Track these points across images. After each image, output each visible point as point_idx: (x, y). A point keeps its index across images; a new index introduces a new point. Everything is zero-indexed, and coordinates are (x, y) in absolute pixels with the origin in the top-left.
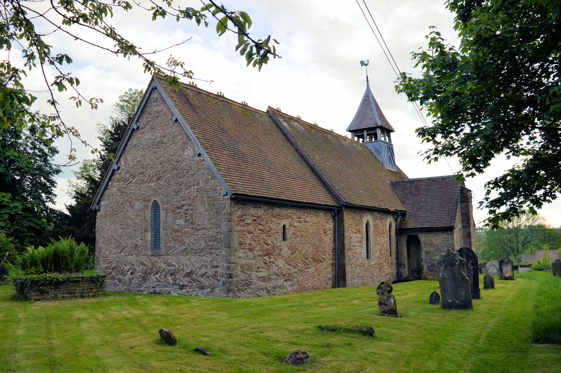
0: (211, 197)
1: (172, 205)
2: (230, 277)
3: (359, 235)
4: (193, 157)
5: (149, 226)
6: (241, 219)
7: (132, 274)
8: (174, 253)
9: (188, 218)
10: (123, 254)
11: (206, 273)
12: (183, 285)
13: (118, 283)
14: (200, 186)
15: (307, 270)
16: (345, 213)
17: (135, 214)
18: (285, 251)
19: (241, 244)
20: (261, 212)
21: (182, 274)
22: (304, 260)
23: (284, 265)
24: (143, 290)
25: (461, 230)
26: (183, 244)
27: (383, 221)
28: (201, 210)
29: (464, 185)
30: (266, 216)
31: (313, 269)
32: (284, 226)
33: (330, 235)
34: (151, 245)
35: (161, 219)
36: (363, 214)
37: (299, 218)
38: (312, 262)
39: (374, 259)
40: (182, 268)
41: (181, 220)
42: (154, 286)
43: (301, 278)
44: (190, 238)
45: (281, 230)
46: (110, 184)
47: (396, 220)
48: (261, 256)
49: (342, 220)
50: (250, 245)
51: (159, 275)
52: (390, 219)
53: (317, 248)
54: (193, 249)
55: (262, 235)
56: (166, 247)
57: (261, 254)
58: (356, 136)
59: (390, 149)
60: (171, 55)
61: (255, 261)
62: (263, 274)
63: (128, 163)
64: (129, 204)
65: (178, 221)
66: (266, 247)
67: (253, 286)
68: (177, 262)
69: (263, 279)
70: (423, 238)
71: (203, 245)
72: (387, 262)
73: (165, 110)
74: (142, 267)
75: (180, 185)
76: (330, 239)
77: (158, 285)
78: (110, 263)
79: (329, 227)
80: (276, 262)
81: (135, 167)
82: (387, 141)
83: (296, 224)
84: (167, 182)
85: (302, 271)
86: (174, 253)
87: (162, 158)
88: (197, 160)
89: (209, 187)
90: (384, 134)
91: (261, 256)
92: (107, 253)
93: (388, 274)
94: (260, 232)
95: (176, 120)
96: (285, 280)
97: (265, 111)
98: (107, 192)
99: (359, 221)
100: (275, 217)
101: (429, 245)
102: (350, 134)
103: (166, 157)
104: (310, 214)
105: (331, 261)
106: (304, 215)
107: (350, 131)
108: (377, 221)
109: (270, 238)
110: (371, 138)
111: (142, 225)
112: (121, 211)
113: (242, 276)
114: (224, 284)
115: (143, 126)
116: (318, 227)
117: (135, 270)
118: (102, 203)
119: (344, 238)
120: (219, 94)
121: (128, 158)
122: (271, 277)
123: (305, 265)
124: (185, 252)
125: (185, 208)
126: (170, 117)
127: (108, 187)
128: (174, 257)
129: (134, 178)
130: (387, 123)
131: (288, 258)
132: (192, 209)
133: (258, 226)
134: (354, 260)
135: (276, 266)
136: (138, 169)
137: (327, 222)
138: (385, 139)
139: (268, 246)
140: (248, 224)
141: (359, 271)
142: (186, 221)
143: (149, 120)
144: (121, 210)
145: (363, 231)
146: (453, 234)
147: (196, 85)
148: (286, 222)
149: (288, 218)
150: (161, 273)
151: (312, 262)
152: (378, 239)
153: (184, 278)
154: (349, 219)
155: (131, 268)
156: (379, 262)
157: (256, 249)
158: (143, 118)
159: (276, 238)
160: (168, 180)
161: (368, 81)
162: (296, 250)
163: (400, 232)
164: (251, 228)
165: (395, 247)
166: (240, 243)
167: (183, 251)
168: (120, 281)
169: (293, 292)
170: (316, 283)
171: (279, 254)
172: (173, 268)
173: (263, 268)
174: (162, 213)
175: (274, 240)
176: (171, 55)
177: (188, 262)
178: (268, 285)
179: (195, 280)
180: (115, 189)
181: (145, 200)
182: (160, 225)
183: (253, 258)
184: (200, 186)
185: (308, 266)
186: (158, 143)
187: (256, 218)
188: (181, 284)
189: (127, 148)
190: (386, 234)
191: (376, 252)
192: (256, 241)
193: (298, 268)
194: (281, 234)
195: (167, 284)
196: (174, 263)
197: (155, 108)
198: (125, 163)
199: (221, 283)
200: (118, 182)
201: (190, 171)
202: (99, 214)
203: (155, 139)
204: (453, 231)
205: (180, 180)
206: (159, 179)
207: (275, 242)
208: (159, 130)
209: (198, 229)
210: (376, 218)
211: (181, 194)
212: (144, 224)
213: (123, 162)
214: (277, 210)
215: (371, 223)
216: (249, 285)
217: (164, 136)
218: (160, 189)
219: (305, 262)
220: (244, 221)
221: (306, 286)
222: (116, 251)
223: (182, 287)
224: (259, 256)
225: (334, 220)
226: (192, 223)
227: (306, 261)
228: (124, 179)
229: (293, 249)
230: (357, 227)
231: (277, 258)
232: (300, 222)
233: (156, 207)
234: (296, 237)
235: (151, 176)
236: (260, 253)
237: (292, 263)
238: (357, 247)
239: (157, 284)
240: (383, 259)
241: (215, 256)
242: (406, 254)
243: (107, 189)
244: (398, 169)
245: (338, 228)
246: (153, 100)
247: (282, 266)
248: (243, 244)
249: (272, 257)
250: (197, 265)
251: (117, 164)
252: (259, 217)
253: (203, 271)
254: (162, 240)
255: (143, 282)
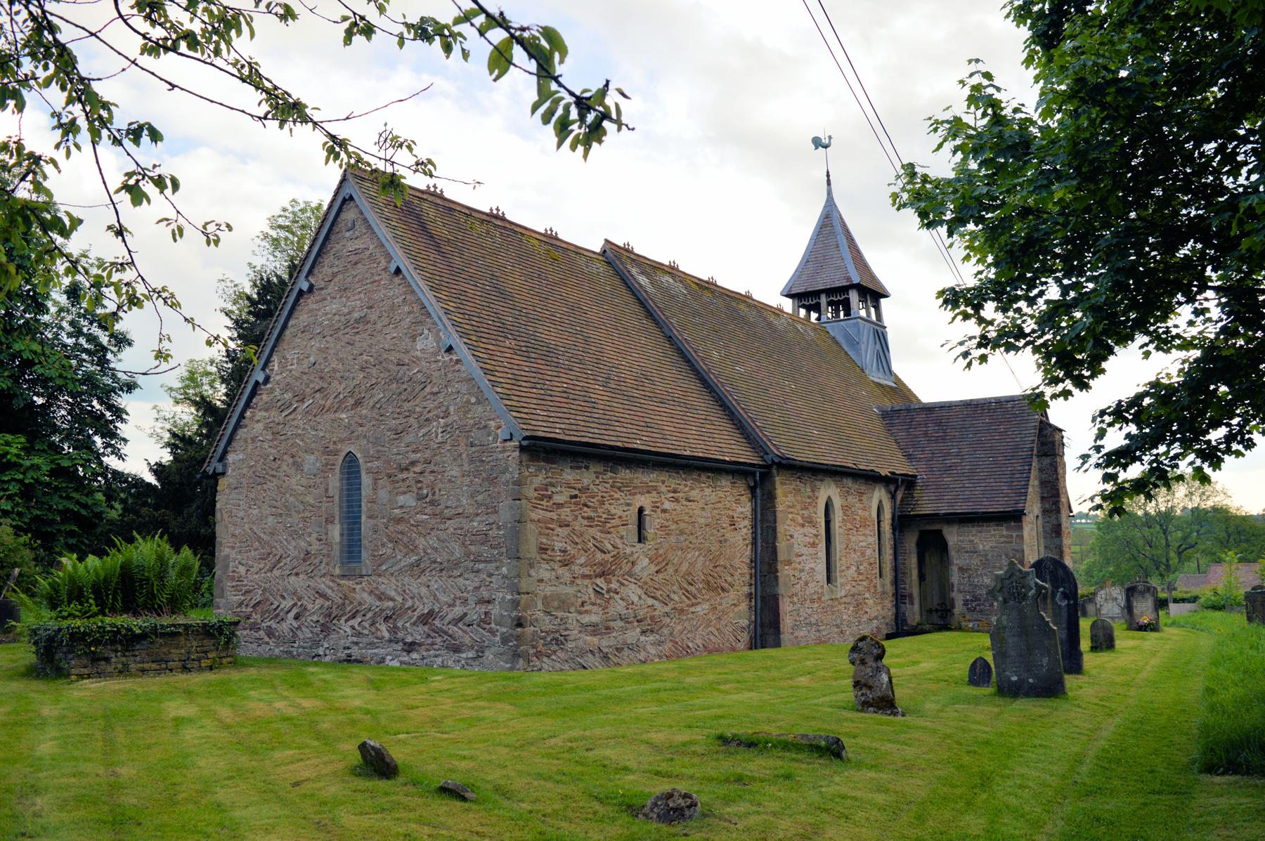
0: (476, 445)
1: (388, 462)
2: (520, 625)
3: (810, 530)
4: (435, 354)
5: (337, 509)
6: (544, 494)
7: (297, 617)
8: (391, 570)
9: (425, 492)
10: (276, 573)
11: (465, 615)
12: (413, 644)
13: (267, 639)
14: (450, 420)
15: (692, 609)
16: (778, 479)
17: (304, 482)
18: (644, 566)
19: (543, 550)
20: (589, 477)
21: (411, 618)
22: (686, 586)
23: (640, 598)
24: (321, 653)
25: (1040, 518)
26: (412, 551)
27: (864, 498)
28: (453, 473)
29: (1047, 418)
30: (599, 487)
31: (706, 606)
32: (641, 510)
33: (745, 531)
34: (341, 552)
35: (363, 493)
36: (818, 483)
37: (675, 491)
38: (704, 591)
39: (842, 585)
40: (409, 603)
41: (407, 496)
42: (347, 645)
43: (679, 627)
44: (428, 537)
45: (635, 518)
46: (248, 414)
47: (893, 497)
48: (589, 577)
49: (771, 497)
50: (564, 551)
51: (359, 620)
52: (879, 495)
53: (715, 559)
54: (435, 562)
55: (591, 530)
56: (375, 556)
57: (587, 573)
58: (804, 306)
59: (880, 336)
60: (386, 125)
61: (575, 588)
62: (594, 618)
63: (289, 367)
64: (291, 460)
65: (401, 499)
66: (599, 556)
67: (570, 645)
68: (399, 590)
69: (594, 629)
70: (953, 536)
71: (458, 552)
72: (872, 591)
73: (371, 247)
74: (320, 601)
75: (406, 417)
76: (745, 539)
77: (357, 643)
78: (247, 592)
79: (742, 513)
80: (622, 590)
81: (305, 377)
82: (874, 317)
83: (667, 505)
84: (376, 411)
85: (682, 611)
86: (391, 570)
87: (365, 357)
88: (444, 362)
89: (472, 421)
90: (866, 302)
91: (589, 577)
92: (242, 570)
93: (876, 618)
94: (586, 522)
95: (398, 271)
96: (643, 632)
97: (598, 250)
98: (241, 433)
99: (809, 497)
100: (619, 488)
101: (967, 552)
102: (789, 301)
103: (375, 355)
104: (699, 482)
105: (746, 589)
106: (686, 486)
107: (789, 296)
108: (850, 498)
109: (609, 536)
110: (837, 312)
111: (320, 507)
112: (273, 476)
113: (547, 623)
114: (505, 640)
115: (323, 284)
116: (716, 511)
117: (306, 609)
118: (231, 458)
119: (775, 538)
120: (495, 212)
121: (288, 356)
122: (612, 624)
123: (688, 598)
124: (416, 568)
125: (417, 469)
126: (383, 263)
127: (244, 422)
128: (393, 580)
129: (302, 401)
130: (873, 277)
131: (649, 581)
132: (433, 472)
133: (581, 509)
134: (798, 586)
135: (622, 599)
136: (312, 381)
137: (737, 502)
138: (868, 313)
139: (603, 556)
140: (560, 506)
141: (809, 611)
142: (420, 498)
143: (335, 270)
144: (274, 473)
145: (818, 520)
146: (1021, 528)
147: (441, 191)
148: (644, 500)
149: (649, 492)
150: (364, 615)
151: (704, 591)
152: (853, 539)
153: (414, 627)
154: (786, 493)
155: (295, 605)
156: (854, 590)
157: (578, 562)
158: (323, 266)
159: (622, 538)
160: (378, 406)
161: (829, 183)
162: (667, 564)
163: (902, 522)
164: (566, 513)
165: (891, 557)
166: (541, 549)
167: (412, 565)
168: (270, 633)
169: (660, 657)
170: (712, 637)
171: (630, 574)
172: (391, 604)
173: (594, 604)
174: (366, 480)
175: (618, 541)
176: (386, 125)
177: (424, 590)
178: (604, 643)
179: (440, 632)
180: (260, 426)
181: (326, 451)
182: (360, 506)
183: (571, 583)
184: (450, 420)
185: (694, 601)
186: (357, 321)
187: (577, 492)
188: (409, 639)
189: (287, 333)
190: (871, 528)
191: (848, 568)
192: (577, 543)
193: (671, 605)
194: (633, 527)
195: (375, 641)
196: (393, 594)
197: (350, 243)
198: (283, 366)
199: (498, 639)
200: (266, 410)
201: (429, 387)
202: (223, 483)
203: (349, 313)
204: (1021, 521)
205: (407, 406)
206: (358, 403)
207: (620, 546)
208: (360, 292)
209: (447, 516)
210: (848, 492)
211: (409, 438)
212: (324, 505)
213: (276, 365)
214: (625, 474)
215: (837, 502)
216: (562, 643)
217: (371, 307)
218: (361, 425)
219: (687, 591)
220: (550, 497)
221: (690, 645)
222: (262, 566)
223: (410, 647)
224: (585, 576)
225: (754, 495)
226: (432, 503)
227: (690, 588)
228: (279, 404)
229: (661, 562)
230: (804, 512)
231: (625, 582)
232: (677, 500)
233: (351, 467)
234: (667, 534)
235: (341, 396)
236: (587, 571)
237: (658, 594)
238: (804, 557)
239: (355, 639)
240: (864, 583)
241: (485, 576)
242: (915, 573)
243: (241, 427)
244: (898, 381)
245: (762, 514)
246: (346, 225)
247: (635, 599)
248: (547, 549)
249: (614, 579)
250: (444, 598)
251: (263, 369)
252: (584, 490)
253: (458, 610)
254: (365, 542)
255: (321, 636)
